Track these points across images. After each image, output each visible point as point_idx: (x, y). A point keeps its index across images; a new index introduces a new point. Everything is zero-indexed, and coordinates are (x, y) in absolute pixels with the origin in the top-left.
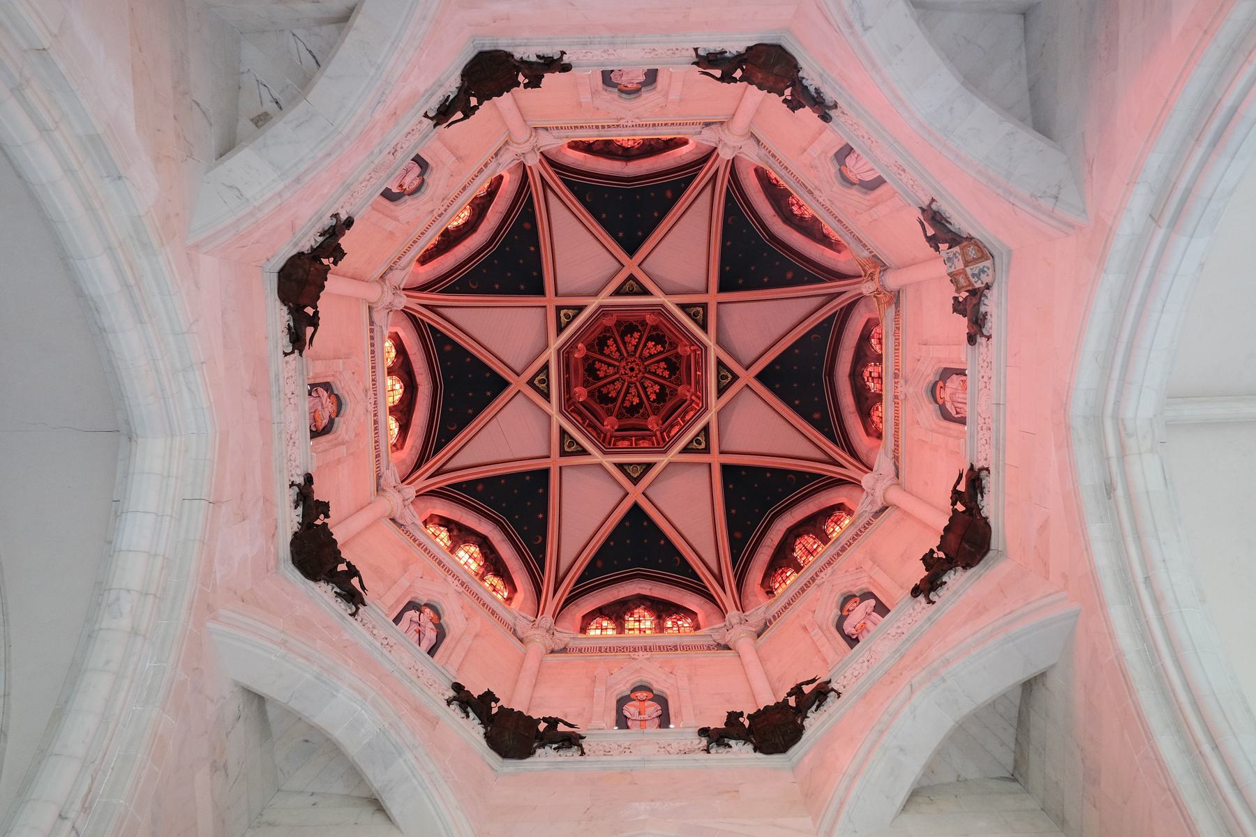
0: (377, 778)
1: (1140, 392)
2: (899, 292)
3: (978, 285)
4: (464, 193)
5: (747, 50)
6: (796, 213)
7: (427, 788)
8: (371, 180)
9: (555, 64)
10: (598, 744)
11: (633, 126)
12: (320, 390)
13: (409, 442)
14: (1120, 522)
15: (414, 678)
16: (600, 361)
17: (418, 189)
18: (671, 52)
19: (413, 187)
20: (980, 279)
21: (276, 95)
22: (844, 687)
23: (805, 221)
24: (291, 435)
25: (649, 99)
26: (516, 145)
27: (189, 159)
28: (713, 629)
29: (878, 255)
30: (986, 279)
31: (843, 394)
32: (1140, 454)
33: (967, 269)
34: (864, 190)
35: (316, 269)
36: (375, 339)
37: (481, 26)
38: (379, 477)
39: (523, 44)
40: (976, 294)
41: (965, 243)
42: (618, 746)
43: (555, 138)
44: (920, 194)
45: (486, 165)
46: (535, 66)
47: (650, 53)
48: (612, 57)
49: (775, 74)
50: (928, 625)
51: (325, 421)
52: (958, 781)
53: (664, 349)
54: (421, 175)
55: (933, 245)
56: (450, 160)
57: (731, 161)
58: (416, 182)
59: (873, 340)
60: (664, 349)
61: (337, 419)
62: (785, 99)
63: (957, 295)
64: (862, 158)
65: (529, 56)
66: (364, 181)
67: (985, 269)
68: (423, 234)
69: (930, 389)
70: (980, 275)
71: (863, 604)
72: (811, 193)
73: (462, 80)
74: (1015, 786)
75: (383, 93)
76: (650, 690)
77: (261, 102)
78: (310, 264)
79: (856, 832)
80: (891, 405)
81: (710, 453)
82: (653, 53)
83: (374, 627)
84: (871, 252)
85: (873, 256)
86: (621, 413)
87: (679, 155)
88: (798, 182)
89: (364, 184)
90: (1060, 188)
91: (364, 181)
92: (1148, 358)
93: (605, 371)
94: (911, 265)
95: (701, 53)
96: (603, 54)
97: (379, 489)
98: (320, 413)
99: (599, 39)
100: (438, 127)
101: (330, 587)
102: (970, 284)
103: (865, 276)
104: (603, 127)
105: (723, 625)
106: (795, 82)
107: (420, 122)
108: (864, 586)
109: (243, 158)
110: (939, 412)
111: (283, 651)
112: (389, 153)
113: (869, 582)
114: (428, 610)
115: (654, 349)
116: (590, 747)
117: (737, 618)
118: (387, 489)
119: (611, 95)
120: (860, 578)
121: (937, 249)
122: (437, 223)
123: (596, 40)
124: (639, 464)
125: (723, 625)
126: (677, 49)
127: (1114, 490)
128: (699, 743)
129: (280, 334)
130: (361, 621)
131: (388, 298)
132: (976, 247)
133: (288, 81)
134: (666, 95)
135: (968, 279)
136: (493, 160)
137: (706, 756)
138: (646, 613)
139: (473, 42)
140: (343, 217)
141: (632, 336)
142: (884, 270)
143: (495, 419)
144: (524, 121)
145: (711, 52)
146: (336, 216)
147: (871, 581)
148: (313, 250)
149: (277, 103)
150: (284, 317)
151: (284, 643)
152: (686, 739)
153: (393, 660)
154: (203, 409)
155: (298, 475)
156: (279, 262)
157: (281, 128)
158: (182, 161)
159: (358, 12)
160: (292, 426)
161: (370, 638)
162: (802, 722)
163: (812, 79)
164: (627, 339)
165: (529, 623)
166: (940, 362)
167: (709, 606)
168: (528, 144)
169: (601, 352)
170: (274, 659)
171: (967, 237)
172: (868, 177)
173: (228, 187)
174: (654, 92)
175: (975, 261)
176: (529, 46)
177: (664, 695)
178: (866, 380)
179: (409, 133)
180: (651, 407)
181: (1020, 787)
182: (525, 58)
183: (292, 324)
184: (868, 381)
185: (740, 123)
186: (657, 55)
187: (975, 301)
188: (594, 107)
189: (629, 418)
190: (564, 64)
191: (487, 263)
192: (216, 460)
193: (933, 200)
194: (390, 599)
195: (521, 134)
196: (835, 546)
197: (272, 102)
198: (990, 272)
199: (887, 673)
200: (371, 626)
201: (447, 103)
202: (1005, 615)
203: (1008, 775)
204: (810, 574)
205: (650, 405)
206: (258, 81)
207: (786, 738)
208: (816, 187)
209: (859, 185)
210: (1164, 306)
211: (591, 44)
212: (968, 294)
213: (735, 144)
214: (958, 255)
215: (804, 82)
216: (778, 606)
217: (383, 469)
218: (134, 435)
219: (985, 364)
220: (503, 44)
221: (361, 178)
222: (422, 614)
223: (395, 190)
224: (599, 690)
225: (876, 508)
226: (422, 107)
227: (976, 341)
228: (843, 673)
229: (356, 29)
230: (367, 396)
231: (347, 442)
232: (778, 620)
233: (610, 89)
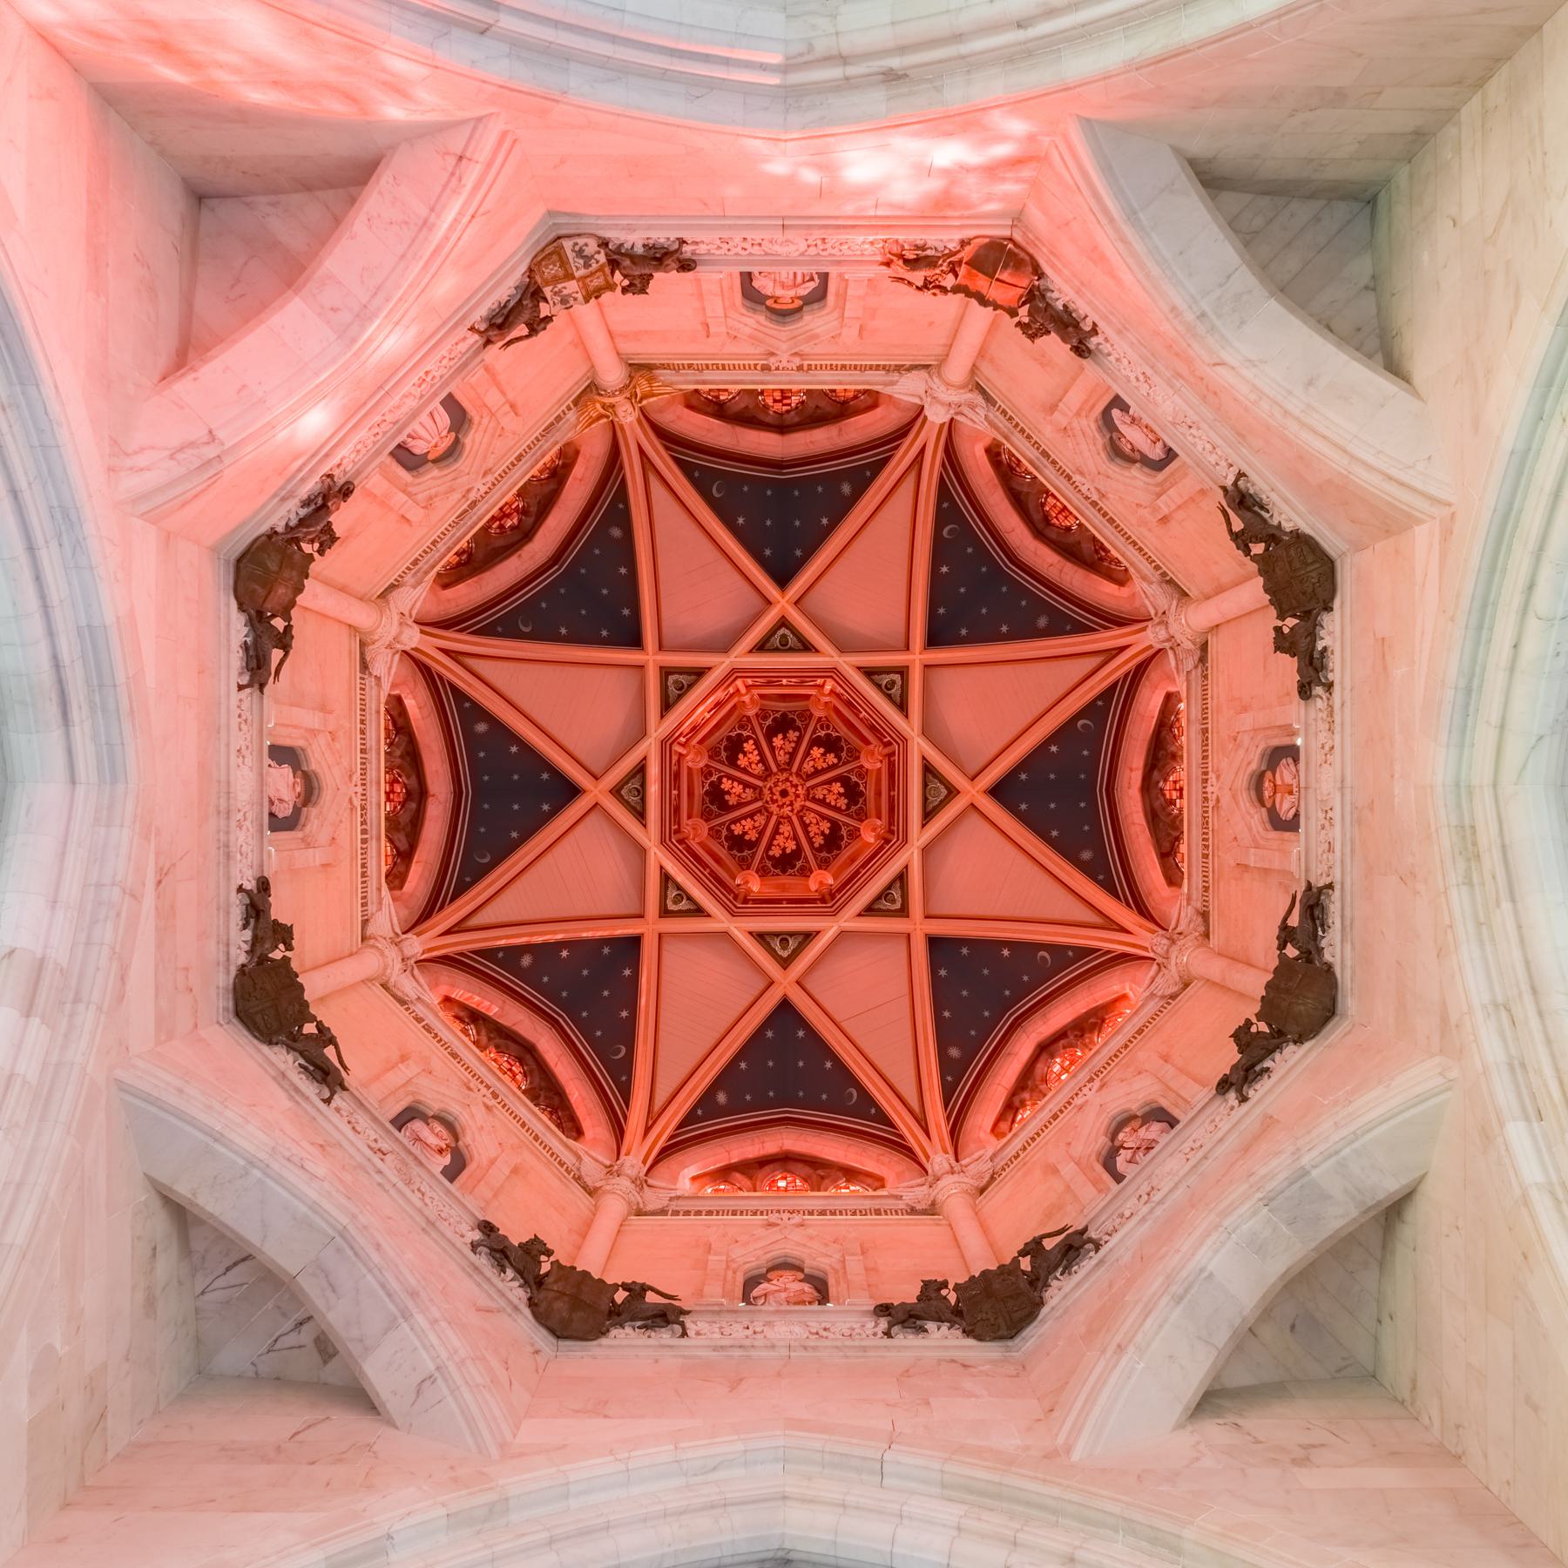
0: (1338, 1216)
1: (745, 35)
2: (630, 365)
3: (602, 258)
4: (463, 1057)
5: (244, 611)
6: (515, 521)
7: (1354, 1133)
8: (423, 1190)
9: (256, 903)
10: (1321, 862)
11: (363, 785)
12: (755, 1293)
13: (869, 1166)
14: (940, 62)
15: (1201, 1154)
16: (769, 847)
17: (450, 1126)
18: (244, 727)
19: (445, 1133)
20: (593, 256)
21: (289, 1324)
22: (1231, 465)
23: (529, 507)
24: (811, 1333)
25: (319, 759)
26: (389, 971)
27: (374, 1448)
28: (1178, 672)
29: (573, 397)
30: (592, 246)
31: (811, 446)
32: (837, 33)
33: (577, 274)
34: (466, 426)
35: (556, 1282)
36: (689, 1209)
37: (196, 1012)
38: (913, 1211)
39: (225, 949)
40: (617, 258)
41: (538, 279)
42: (1323, 829)
43: (381, 909)
44: (463, 347)
45: (419, 1020)
46: (260, 934)
47: (243, 757)
48: (249, 816)
49: (280, 568)
50: (1128, 334)
51: (807, 1287)
52: (1374, 290)
53: (751, 737)
54: (425, 1118)
55: (542, 325)
56: (409, 1070)
57: (422, 627)
58: (438, 1128)
59: (722, 398)
60: (751, 737)
61: (806, 1271)
62: (318, 551)
63: (619, 289)
64: (413, 431)
65: (245, 942)
66: (423, 1200)
67: (577, 248)
68: (523, 1125)
69: (780, 319)
70: (586, 256)
71: (1122, 428)
72: (474, 504)
73: (277, 1044)
74: (1382, 201)
75: (289, 1160)
76: (1261, 775)
77: (300, 1347)
78: (547, 1289)
79: (1430, 458)
80: (815, 375)
81: (908, 667)
82: (244, 751)
83: (1122, 1216)
84: (569, 408)
85: (575, 405)
86: (857, 814)
87: (417, 710)
88: (457, 523)
89: (428, 1201)
90: (447, 153)
91: (423, 1200)
92: (691, 26)
93: (787, 839)
94: (585, 350)
95: (245, 680)
96: (244, 828)
97: (932, 1210)
98: (792, 1294)
99: (221, 834)
100: (346, 1084)
101: (1054, 1283)
102: (601, 269)
103: (607, 417)
104: (364, 832)
105: (1170, 653)
106: (292, 538)
107: (338, 1110)
108: (1093, 426)
109: (378, 1374)
110: (816, 306)
111: (1131, 1349)
112: (382, 1160)
113: (1086, 417)
114: (1121, 1136)
115: (750, 756)
116: (1324, 875)
117: (1158, 628)
118: (932, 1198)
119: (312, 818)
120: (1082, 430)
121: (548, 319)
122: (507, 1102)
123: (222, 839)
124: (925, 785)
125: (1170, 653)
126: (240, 716)
127: (892, 70)
128: (1321, 698)
129: (651, 1342)
130: (1110, 1235)
131: (624, 1184)
132: (543, 263)
133: (270, 1305)
134: (313, 732)
135: (592, 274)
136: (412, 1008)
137: (1337, 689)
138: (1171, 779)
139: (221, 1025)
140: (477, 1236)
141: (729, 793)
142: (597, 389)
143: (844, 1025)
144: (351, 955)
145: (244, 664)
146: (474, 1247)
147: (1084, 414)
148: (526, 1284)
149: (301, 1324)
150: (627, 1334)
151: (1120, 1348)
152: (1315, 720)
153: (1172, 1184)
154: (746, 1451)
155: (877, 1325)
156: (541, 1337)
157: (336, 1316)
158: (376, 1457)
159: (171, 1189)
160: (797, 1329)
161: (1135, 1220)
162: (1286, 533)
163: (289, 511)
164: (732, 800)
165: (1161, 974)
166: (734, 305)
167: (1153, 674)
168: (387, 952)
169: (753, 845)
170: (1142, 1365)
171: (529, 277)
172: (444, 420)
173: (418, 1396)
174: (309, 751)
175: (564, 263)
176: (228, 940)
177: (1268, 752)
178: (789, 408)
179: (353, 1128)
180: (848, 762)
181: (1383, 191)
182: (246, 947)
183: (639, 1323)
184: (790, 405)
185: (362, 616)
186: (247, 747)
187: (627, 262)
188: (330, 845)
189: (865, 800)
190: (258, 889)
191: (585, 1029)
192: (827, 1437)
193: (472, 329)
194: (1087, 1192)
195: (369, 963)
196: (1041, 466)
197: (299, 1332)
198: (581, 241)
199: (1204, 398)
200: (1118, 1220)
201: (311, 1068)
202: (1099, 222)
203: (1368, 210)
204: (1087, 508)
205: (844, 764)
206: (269, 1351)
207: (1309, 561)
208: (464, 496)
209: (457, 432)
210: (615, 9)
211: (228, 847)
212: (617, 272)
213: (396, 623)
214: (556, 289)
215: (293, 523)
216: (1140, 561)
217: (901, 1205)
218: (780, 1554)
219: (725, 246)
220: (224, 979)
221: (419, 1204)
222: (1125, 1145)
223: (446, 1160)
224: (1252, 858)
225: (980, 400)
226: (314, 1106)
227: (690, 260)
228: (1211, 467)
229: (194, 1194)
230: (778, 1225)
231: (843, 1256)
232: (1158, 562)
233: (302, 819)
